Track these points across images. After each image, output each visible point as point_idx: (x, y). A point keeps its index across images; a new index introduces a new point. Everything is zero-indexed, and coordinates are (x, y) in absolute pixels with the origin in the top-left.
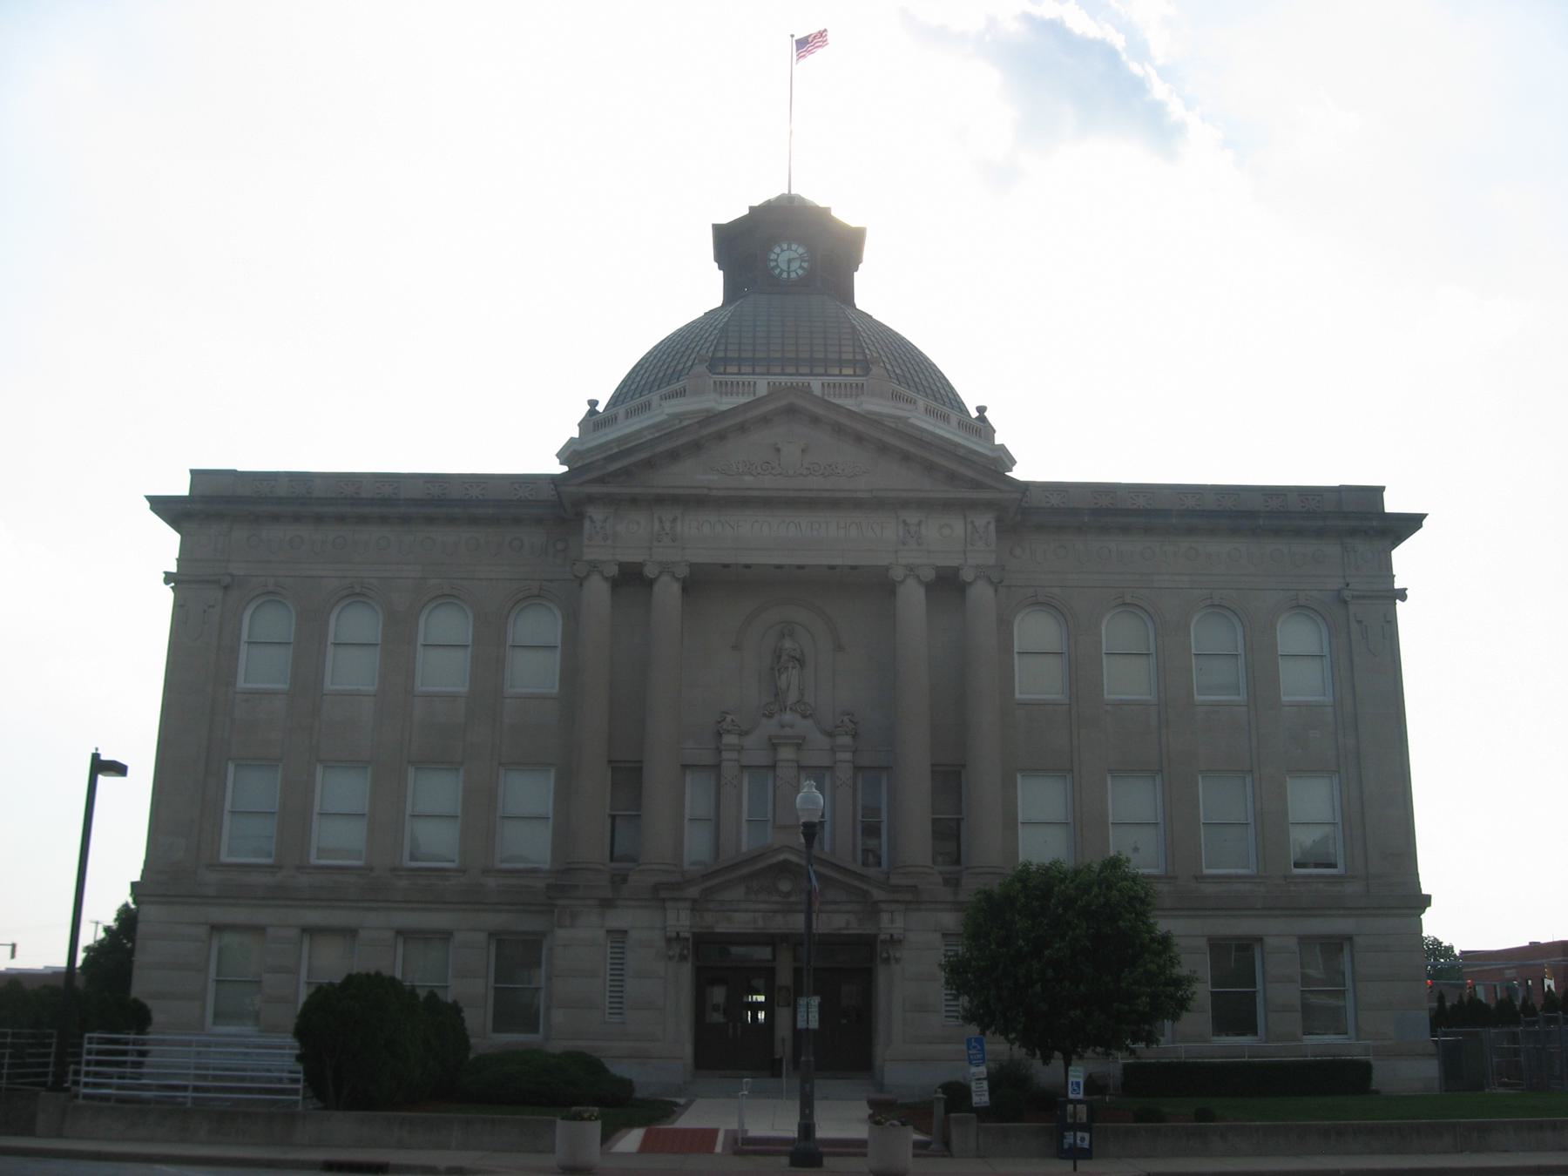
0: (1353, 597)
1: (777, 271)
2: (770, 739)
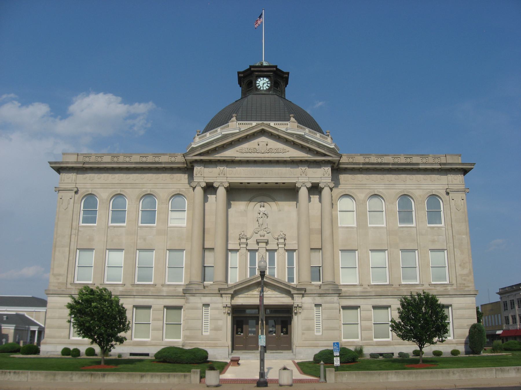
1: (259, 87)
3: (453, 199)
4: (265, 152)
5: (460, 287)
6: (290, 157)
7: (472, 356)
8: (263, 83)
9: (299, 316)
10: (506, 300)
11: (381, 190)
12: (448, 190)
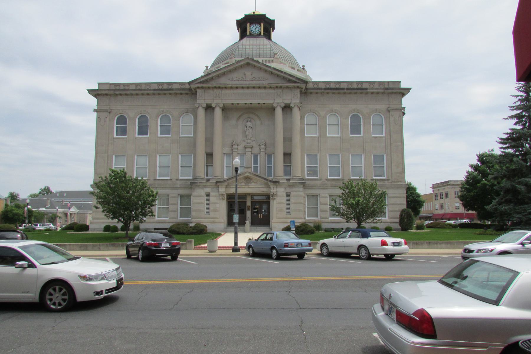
0: (391, 110)
2: (245, 146)
3: (393, 116)
5: (395, 181)
8: (253, 28)
9: (275, 201)
10: (437, 193)
11: (338, 109)
12: (389, 109)
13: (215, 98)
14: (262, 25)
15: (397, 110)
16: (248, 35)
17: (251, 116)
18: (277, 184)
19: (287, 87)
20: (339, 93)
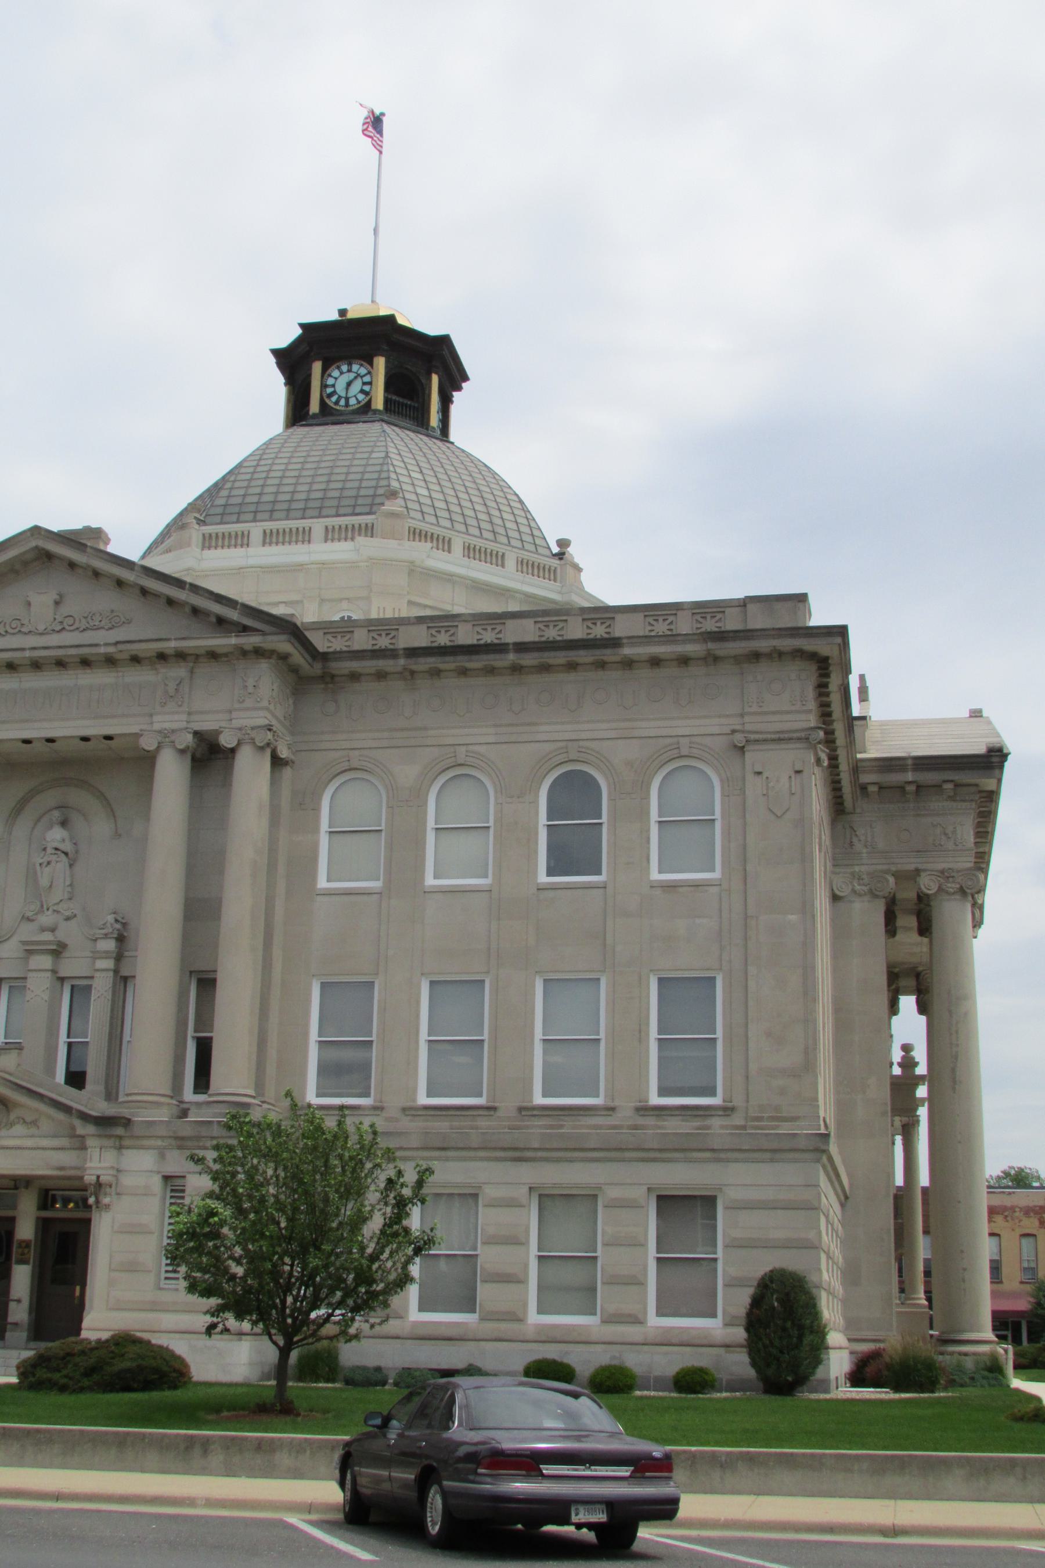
3: (759, 773)
4: (50, 628)
6: (117, 643)
7: (726, 1399)
11: (482, 749)
13: (237, 706)
14: (380, 362)
15: (780, 740)
16: (315, 416)
17: (78, 797)
18: (120, 1131)
19: (213, 655)
20: (491, 671)
